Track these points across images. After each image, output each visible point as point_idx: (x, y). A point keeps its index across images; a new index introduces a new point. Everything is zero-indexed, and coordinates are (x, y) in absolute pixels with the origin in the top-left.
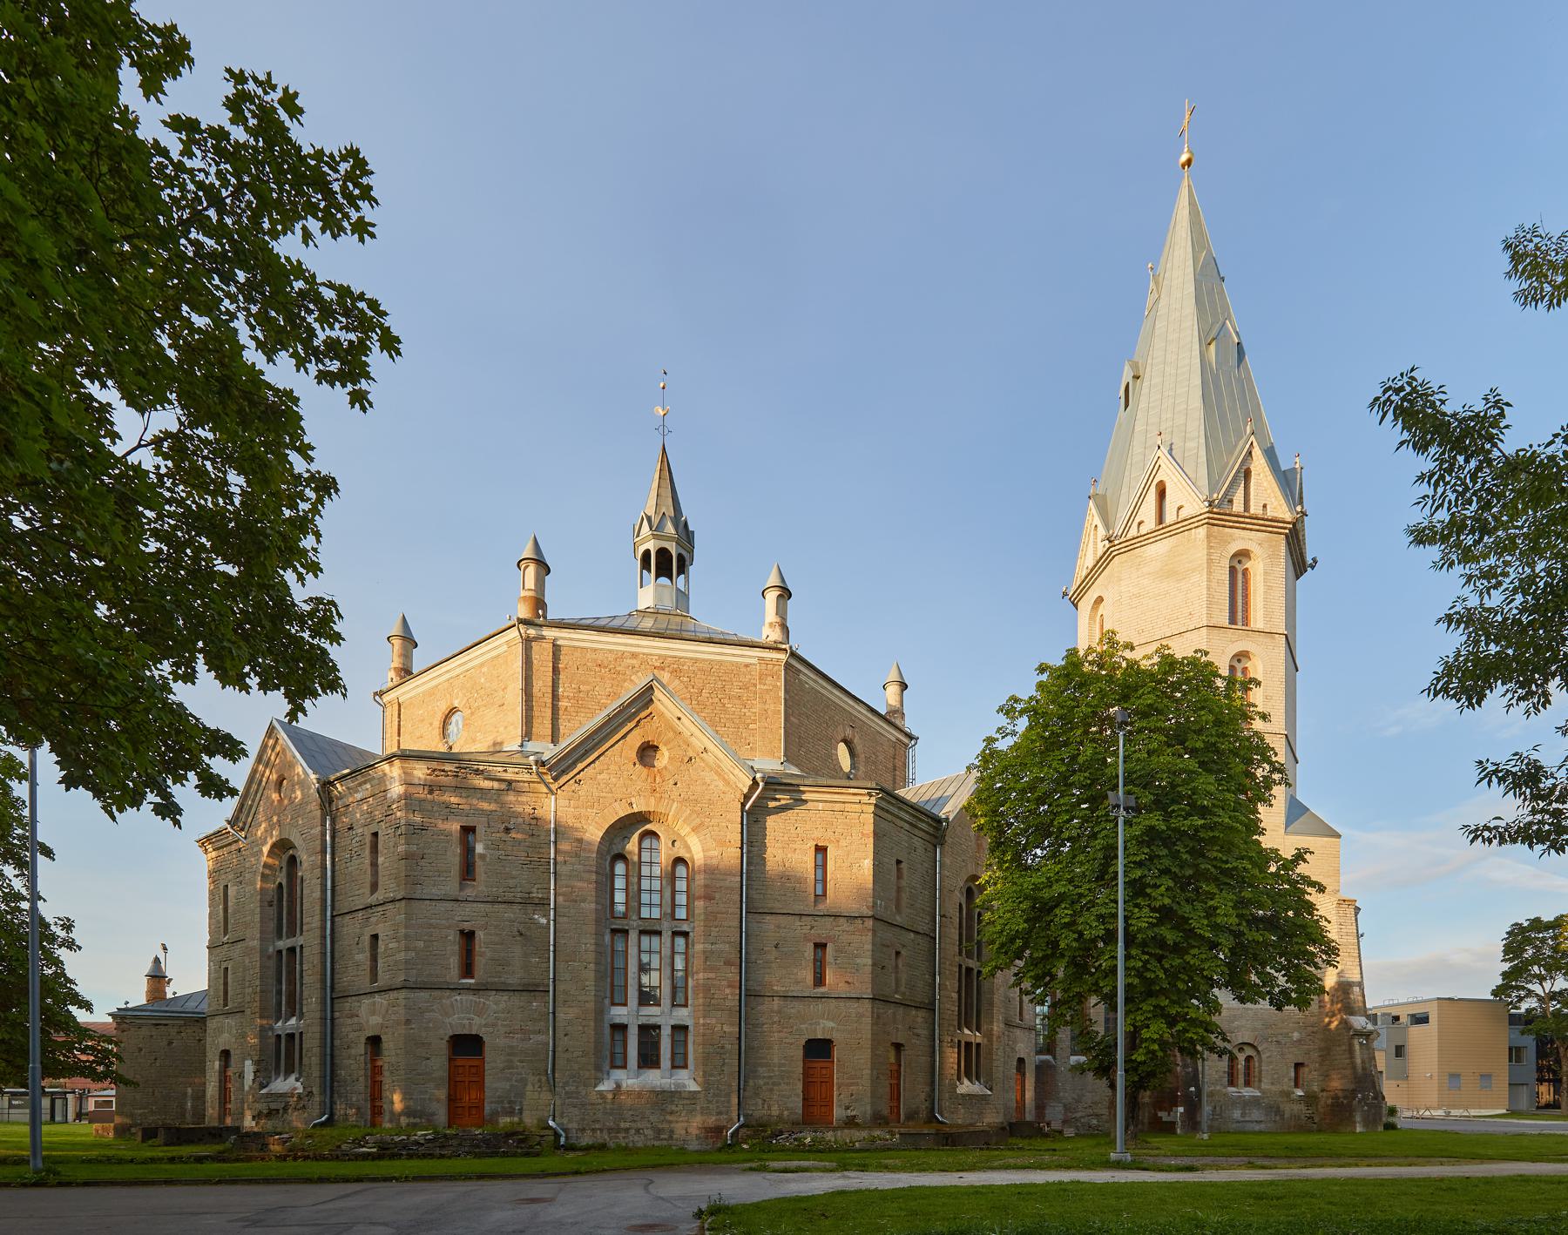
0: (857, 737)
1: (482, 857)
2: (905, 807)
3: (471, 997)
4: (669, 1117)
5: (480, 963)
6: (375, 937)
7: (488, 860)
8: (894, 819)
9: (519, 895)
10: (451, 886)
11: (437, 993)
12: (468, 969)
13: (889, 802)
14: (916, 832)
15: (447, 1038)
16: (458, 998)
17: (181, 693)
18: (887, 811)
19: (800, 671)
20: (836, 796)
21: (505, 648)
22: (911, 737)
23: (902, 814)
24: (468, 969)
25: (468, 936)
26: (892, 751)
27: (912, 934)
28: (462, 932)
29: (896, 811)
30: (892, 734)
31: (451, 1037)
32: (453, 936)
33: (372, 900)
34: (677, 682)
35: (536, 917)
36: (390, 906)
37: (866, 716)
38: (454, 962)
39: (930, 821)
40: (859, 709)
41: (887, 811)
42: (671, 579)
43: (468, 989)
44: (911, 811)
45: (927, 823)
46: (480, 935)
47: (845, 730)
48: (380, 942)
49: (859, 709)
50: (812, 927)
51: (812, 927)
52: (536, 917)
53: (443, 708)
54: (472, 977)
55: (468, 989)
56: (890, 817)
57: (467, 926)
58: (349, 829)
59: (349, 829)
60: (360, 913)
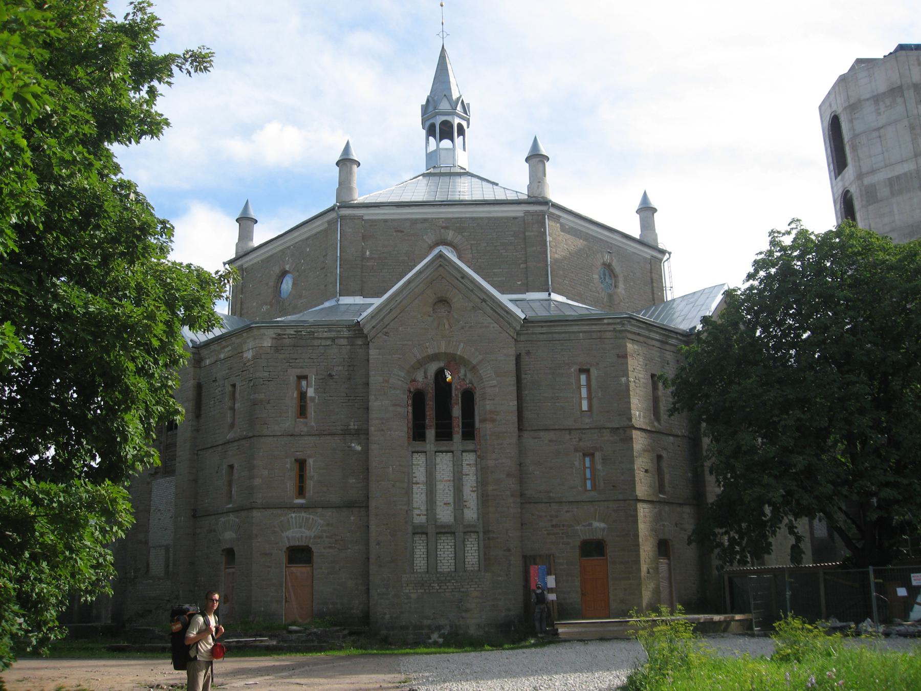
0: (615, 261)
1: (313, 399)
2: (655, 329)
3: (303, 514)
4: (464, 614)
5: (310, 485)
6: (231, 467)
7: (317, 401)
8: (646, 340)
9: (339, 428)
10: (289, 422)
11: (275, 511)
12: (301, 492)
13: (640, 327)
14: (668, 347)
15: (284, 549)
16: (293, 515)
17: (294, 502)
18: (639, 334)
19: (560, 217)
20: (594, 327)
21: (326, 225)
22: (663, 252)
23: (653, 335)
24: (301, 492)
25: (301, 464)
26: (648, 266)
27: (671, 438)
28: (297, 460)
29: (647, 333)
30: (646, 253)
31: (287, 548)
32: (289, 464)
33: (230, 436)
34: (460, 237)
35: (353, 445)
36: (243, 442)
37: (620, 242)
38: (290, 486)
39: (679, 337)
40: (614, 237)
41: (639, 334)
42: (452, 140)
43: (301, 507)
44: (659, 331)
45: (677, 339)
46: (310, 462)
47: (603, 257)
48: (235, 471)
49: (614, 237)
50: (580, 440)
51: (580, 440)
52: (353, 445)
53: (277, 270)
54: (304, 498)
55: (301, 507)
56: (641, 339)
57: (299, 455)
58: (214, 381)
59: (214, 381)
60: (220, 448)
